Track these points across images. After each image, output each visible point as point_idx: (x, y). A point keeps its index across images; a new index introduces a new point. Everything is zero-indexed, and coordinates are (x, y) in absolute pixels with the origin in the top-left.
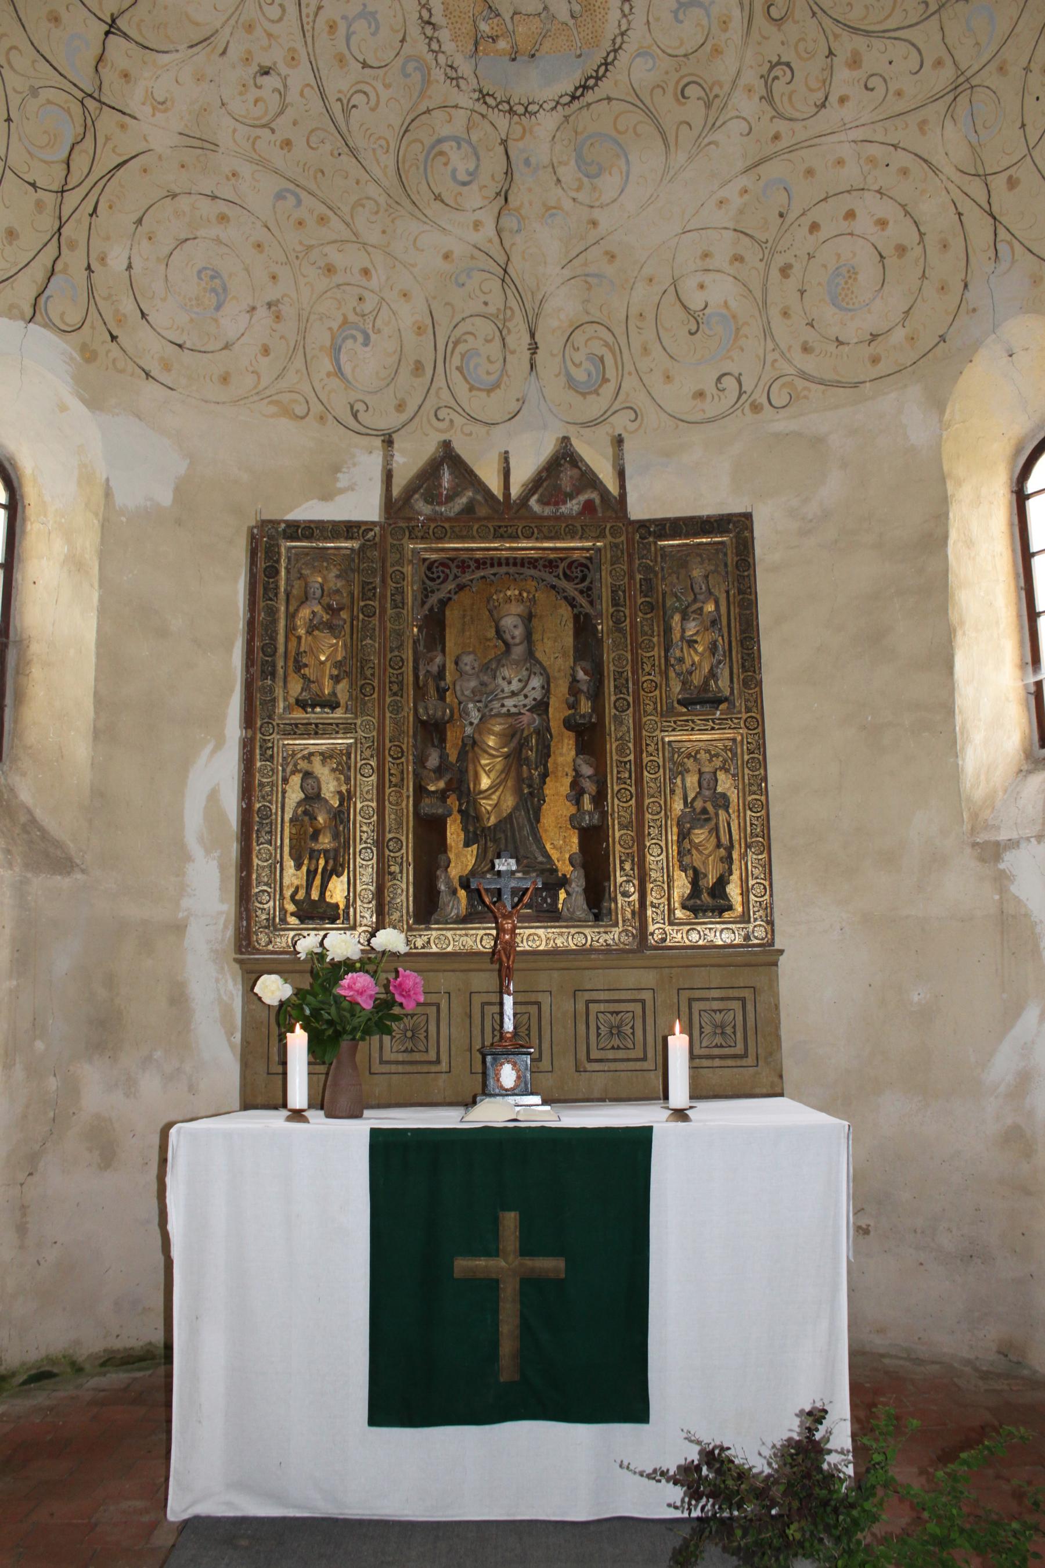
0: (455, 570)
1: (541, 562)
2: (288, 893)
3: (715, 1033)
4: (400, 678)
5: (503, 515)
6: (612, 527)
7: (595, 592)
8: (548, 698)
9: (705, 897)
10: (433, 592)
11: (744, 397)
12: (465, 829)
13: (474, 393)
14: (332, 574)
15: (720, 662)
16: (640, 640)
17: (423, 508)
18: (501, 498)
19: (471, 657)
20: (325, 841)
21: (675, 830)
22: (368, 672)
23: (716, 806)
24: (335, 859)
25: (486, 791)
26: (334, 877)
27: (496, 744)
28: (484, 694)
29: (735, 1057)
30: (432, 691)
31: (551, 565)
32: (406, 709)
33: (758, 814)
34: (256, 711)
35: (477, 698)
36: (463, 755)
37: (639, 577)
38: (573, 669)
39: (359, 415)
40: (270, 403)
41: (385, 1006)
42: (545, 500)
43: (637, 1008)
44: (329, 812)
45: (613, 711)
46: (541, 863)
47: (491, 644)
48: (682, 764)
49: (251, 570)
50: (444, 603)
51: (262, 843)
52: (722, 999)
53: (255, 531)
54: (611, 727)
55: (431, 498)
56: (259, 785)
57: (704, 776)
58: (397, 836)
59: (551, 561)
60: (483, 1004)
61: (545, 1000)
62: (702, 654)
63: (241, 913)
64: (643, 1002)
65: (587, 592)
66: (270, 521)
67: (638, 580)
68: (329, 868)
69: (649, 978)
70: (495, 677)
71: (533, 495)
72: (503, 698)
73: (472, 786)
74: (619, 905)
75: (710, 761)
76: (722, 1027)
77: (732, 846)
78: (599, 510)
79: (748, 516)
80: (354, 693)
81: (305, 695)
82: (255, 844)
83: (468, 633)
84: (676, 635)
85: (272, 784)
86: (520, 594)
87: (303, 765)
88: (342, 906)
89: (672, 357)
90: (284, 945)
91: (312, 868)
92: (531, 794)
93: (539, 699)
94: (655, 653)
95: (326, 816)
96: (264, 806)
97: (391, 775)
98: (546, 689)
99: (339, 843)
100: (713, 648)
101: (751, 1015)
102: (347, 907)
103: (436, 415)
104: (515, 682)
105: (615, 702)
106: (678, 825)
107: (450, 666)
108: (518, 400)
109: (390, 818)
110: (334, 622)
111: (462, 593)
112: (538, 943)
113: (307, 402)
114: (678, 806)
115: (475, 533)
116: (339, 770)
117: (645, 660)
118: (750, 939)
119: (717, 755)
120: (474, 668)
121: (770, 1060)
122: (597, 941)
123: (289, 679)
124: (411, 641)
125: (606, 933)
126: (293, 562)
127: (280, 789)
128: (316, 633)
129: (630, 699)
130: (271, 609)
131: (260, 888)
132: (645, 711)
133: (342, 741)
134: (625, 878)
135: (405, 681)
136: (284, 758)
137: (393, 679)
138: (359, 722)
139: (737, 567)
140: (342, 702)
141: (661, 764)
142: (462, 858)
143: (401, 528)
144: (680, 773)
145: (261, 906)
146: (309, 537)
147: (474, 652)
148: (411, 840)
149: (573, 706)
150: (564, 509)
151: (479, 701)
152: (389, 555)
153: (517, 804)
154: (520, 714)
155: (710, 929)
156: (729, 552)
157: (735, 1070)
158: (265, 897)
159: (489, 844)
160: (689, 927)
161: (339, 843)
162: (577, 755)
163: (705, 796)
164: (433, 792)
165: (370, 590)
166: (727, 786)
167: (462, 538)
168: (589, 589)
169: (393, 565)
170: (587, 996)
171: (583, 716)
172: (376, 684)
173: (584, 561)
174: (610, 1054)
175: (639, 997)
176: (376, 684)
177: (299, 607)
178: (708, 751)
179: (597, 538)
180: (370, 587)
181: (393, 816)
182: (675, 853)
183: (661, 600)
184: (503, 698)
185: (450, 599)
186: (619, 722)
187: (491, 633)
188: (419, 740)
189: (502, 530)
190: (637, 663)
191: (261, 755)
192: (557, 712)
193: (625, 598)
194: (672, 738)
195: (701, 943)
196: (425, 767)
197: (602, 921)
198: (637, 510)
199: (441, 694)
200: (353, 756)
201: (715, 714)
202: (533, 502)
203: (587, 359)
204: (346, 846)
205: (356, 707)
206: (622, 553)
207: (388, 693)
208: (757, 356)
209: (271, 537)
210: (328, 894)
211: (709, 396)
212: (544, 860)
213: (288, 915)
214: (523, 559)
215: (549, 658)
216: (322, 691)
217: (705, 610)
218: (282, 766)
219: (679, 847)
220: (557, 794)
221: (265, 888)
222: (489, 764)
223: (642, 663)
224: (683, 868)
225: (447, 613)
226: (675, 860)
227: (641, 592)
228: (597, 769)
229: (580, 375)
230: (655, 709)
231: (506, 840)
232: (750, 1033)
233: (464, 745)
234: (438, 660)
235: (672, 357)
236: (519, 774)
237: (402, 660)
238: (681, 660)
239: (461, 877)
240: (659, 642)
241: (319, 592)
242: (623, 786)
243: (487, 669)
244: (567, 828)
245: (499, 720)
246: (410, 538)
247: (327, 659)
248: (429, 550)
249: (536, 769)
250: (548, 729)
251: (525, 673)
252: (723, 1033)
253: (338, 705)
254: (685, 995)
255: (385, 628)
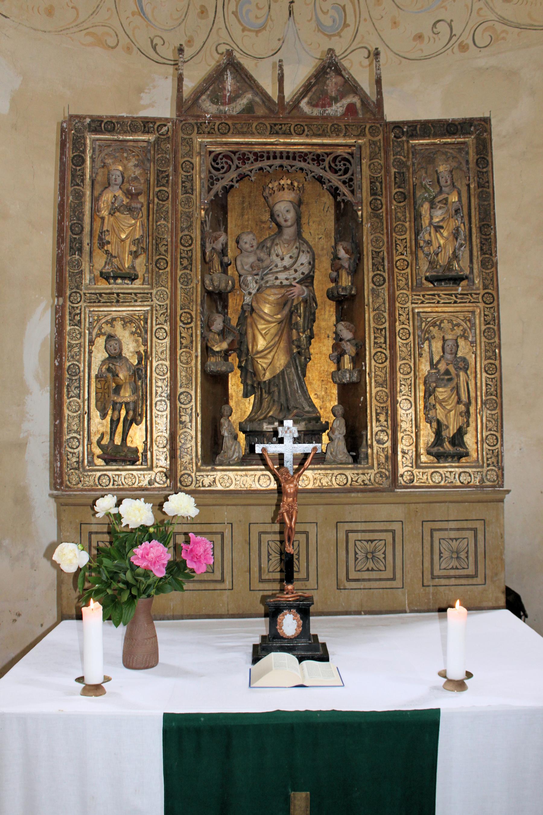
0: (236, 162)
1: (310, 156)
2: (95, 439)
3: (452, 558)
4: (190, 254)
5: (278, 115)
6: (371, 127)
7: (356, 182)
8: (314, 272)
9: (447, 445)
10: (218, 180)
11: (454, 39)
12: (244, 382)
13: (246, 33)
14: (131, 164)
15: (461, 245)
16: (395, 225)
17: (209, 108)
18: (276, 100)
19: (251, 236)
20: (126, 395)
21: (422, 387)
22: (162, 249)
23: (458, 368)
24: (135, 410)
25: (262, 351)
26: (134, 424)
27: (271, 311)
28: (261, 270)
29: (467, 577)
30: (217, 265)
31: (318, 159)
32: (195, 281)
33: (493, 376)
34: (64, 280)
35: (255, 272)
36: (242, 319)
37: (393, 170)
38: (335, 248)
39: (157, 47)
40: (88, 34)
41: (177, 569)
42: (314, 103)
43: (388, 536)
44: (129, 370)
45: (371, 285)
46: (308, 412)
47: (266, 226)
48: (428, 332)
49: (61, 159)
50: (227, 190)
51: (72, 397)
52: (458, 529)
53: (65, 125)
54: (368, 297)
55: (216, 99)
56: (69, 347)
57: (448, 343)
58: (187, 390)
59: (318, 156)
60: (260, 533)
61: (312, 529)
62: (447, 239)
63: (55, 455)
64: (393, 532)
65: (348, 183)
66: (77, 116)
67: (393, 173)
68: (129, 418)
69: (398, 512)
70: (269, 255)
71: (303, 98)
72: (277, 272)
73: (250, 347)
74: (375, 451)
75: (452, 330)
76: (458, 552)
77: (469, 403)
78: (360, 112)
79: (486, 121)
80: (150, 267)
81: (108, 269)
82: (65, 397)
83: (246, 217)
84: (426, 222)
85: (80, 346)
86: (292, 183)
87: (107, 329)
88: (141, 450)
89: (398, 7)
90: (92, 483)
91: (115, 418)
92: (299, 353)
93: (306, 273)
94: (407, 236)
95: (126, 373)
96: (73, 364)
97: (182, 337)
98: (312, 265)
99: (138, 396)
100: (456, 235)
101: (481, 544)
102: (145, 450)
103: (217, 50)
104: (287, 258)
105: (373, 277)
106: (425, 383)
107: (232, 244)
108: (279, 40)
109: (181, 374)
110: (133, 205)
111: (241, 183)
112: (307, 482)
113: (117, 35)
114: (425, 368)
115: (254, 130)
116: (138, 333)
117: (398, 242)
118: (484, 482)
119: (458, 325)
120: (252, 247)
121: (495, 579)
122: (356, 481)
123: (94, 254)
124: (199, 222)
125: (364, 474)
126: (97, 153)
127: (87, 350)
128: (117, 214)
129: (386, 275)
130: (78, 193)
131: (71, 435)
132: (398, 286)
133: (140, 309)
134: (380, 428)
135: (194, 257)
136: (90, 323)
137: (183, 255)
138: (154, 292)
139: (477, 164)
140: (140, 275)
141: (411, 331)
142: (241, 406)
143: (191, 124)
144: (428, 339)
145: (72, 451)
146: (112, 131)
147: (251, 232)
148: (199, 394)
149: (335, 280)
150: (330, 111)
151: (257, 275)
152: (180, 147)
153: (289, 363)
154: (291, 285)
155: (451, 472)
156: (471, 152)
157: (468, 587)
158: (75, 443)
159: (265, 396)
160: (433, 470)
161: (138, 396)
162: (338, 321)
163: (447, 360)
164: (217, 352)
165: (163, 177)
166: (467, 351)
167: (243, 134)
168: (351, 180)
169: (183, 157)
170: (347, 527)
171: (344, 289)
172: (169, 259)
173: (347, 156)
174: (366, 575)
175: (390, 528)
176: (169, 259)
177: (103, 191)
178: (450, 321)
179: (358, 136)
180: (164, 175)
181: (184, 374)
182: (422, 407)
183: (412, 191)
184: (277, 272)
185: (232, 186)
186: (375, 294)
187: (266, 217)
188: (206, 306)
189: (278, 128)
190: (392, 244)
191: (70, 320)
192: (321, 285)
193: (381, 188)
194: (421, 310)
195: (442, 483)
196: (211, 330)
197: (360, 463)
198: (395, 111)
199: (225, 267)
200: (149, 321)
201: (457, 290)
202: (303, 104)
203: (333, 8)
204: (144, 398)
205: (152, 279)
206: (380, 150)
207: (179, 267)
208: (466, 6)
209: (78, 130)
210: (129, 439)
211: (426, 40)
212: (311, 410)
213: (95, 458)
214: (294, 153)
215: (314, 238)
216: (123, 264)
217: (449, 200)
218: (89, 329)
219: (425, 403)
220: (320, 353)
221: (75, 435)
222: (265, 328)
223: (396, 244)
224: (429, 420)
225: (229, 199)
226: (422, 413)
227: (395, 183)
228: (355, 333)
229: (327, 21)
230: (407, 284)
231: (279, 392)
232: (480, 557)
233: (244, 311)
234: (222, 239)
235: (398, 7)
236: (290, 336)
237: (191, 238)
238: (429, 243)
239: (240, 424)
240: (410, 227)
241: (120, 180)
242: (379, 350)
243: (263, 247)
244: (328, 382)
245: (273, 291)
246: (198, 133)
247: (127, 238)
248: (218, 143)
249: (304, 332)
250: (314, 299)
251: (295, 251)
252: (458, 558)
253: (136, 277)
254: (428, 526)
255: (176, 211)
